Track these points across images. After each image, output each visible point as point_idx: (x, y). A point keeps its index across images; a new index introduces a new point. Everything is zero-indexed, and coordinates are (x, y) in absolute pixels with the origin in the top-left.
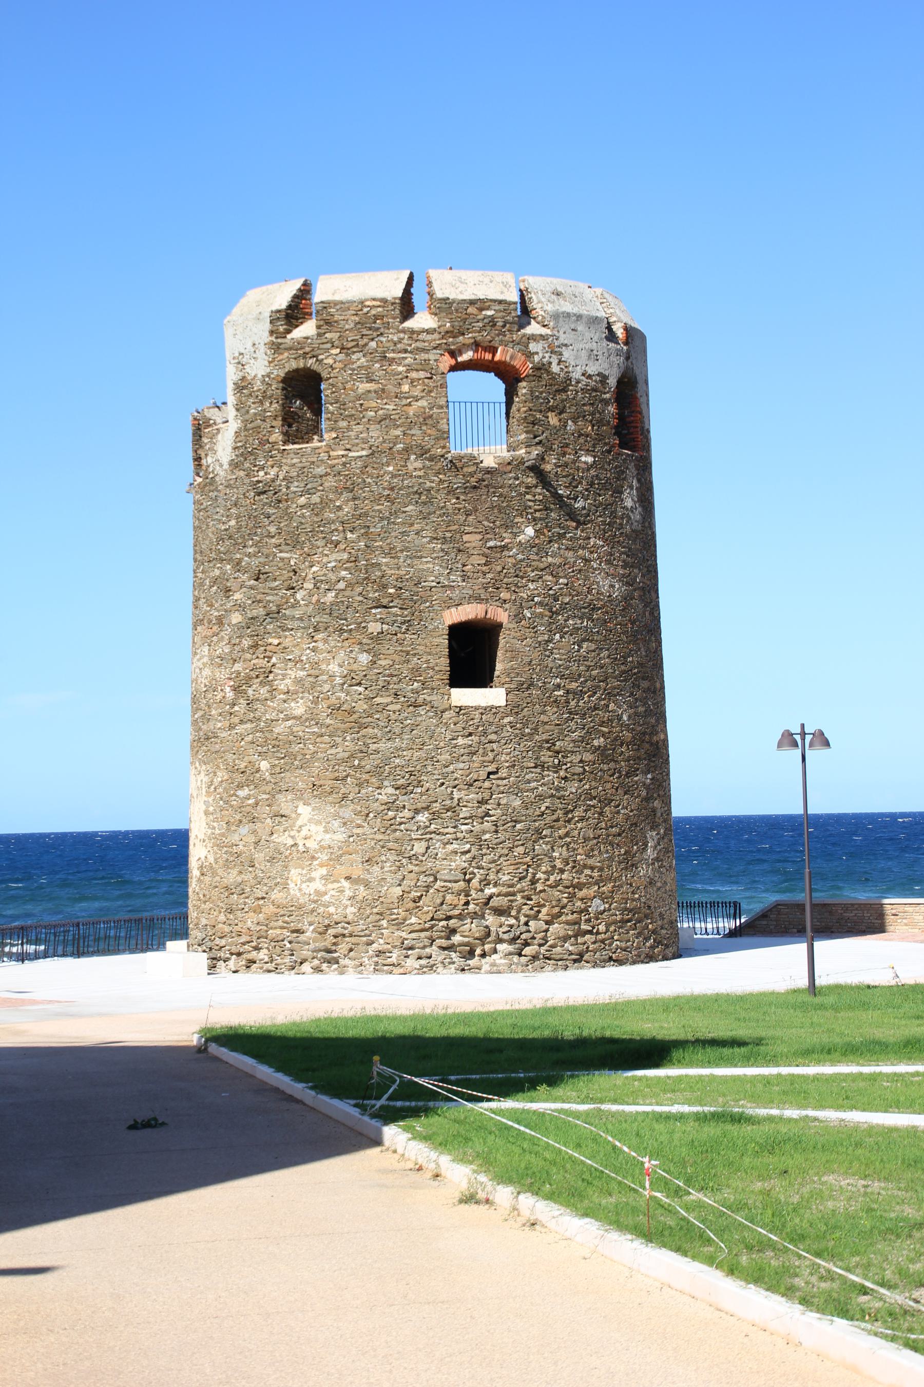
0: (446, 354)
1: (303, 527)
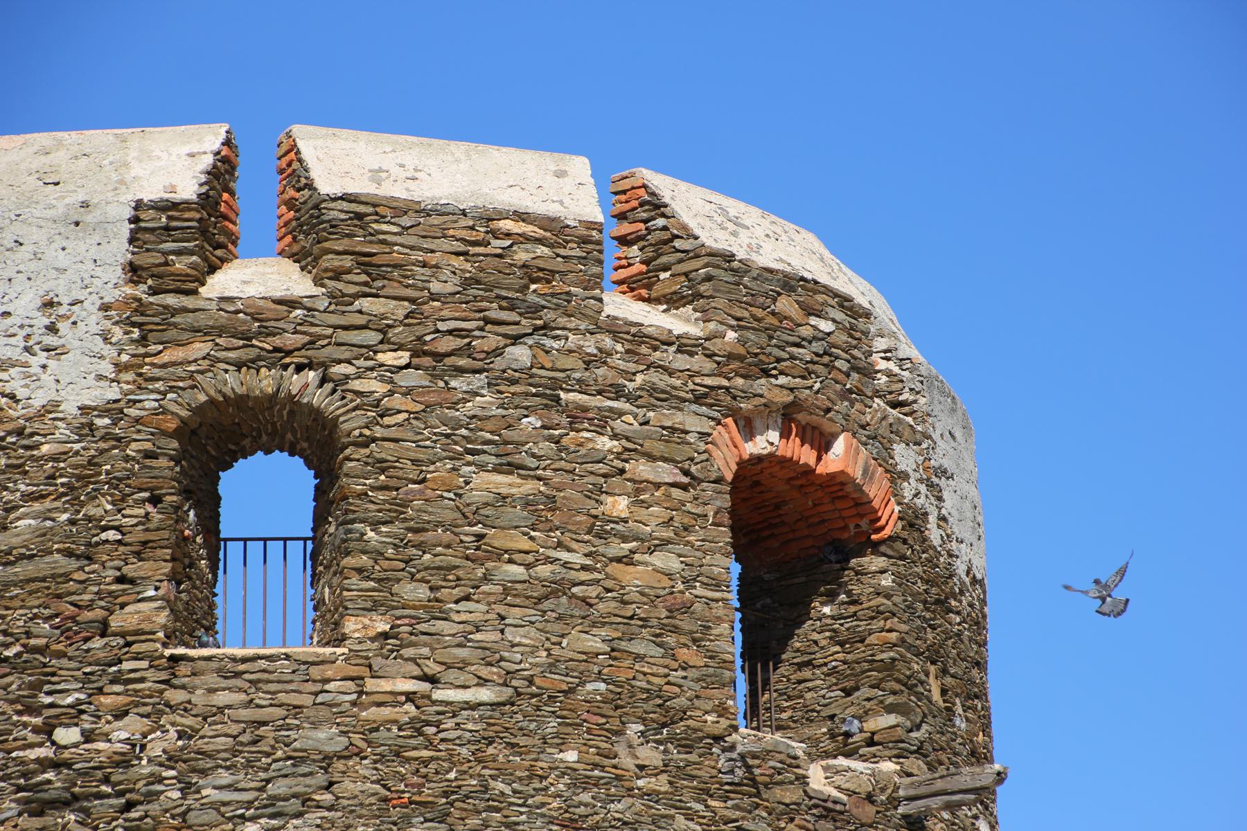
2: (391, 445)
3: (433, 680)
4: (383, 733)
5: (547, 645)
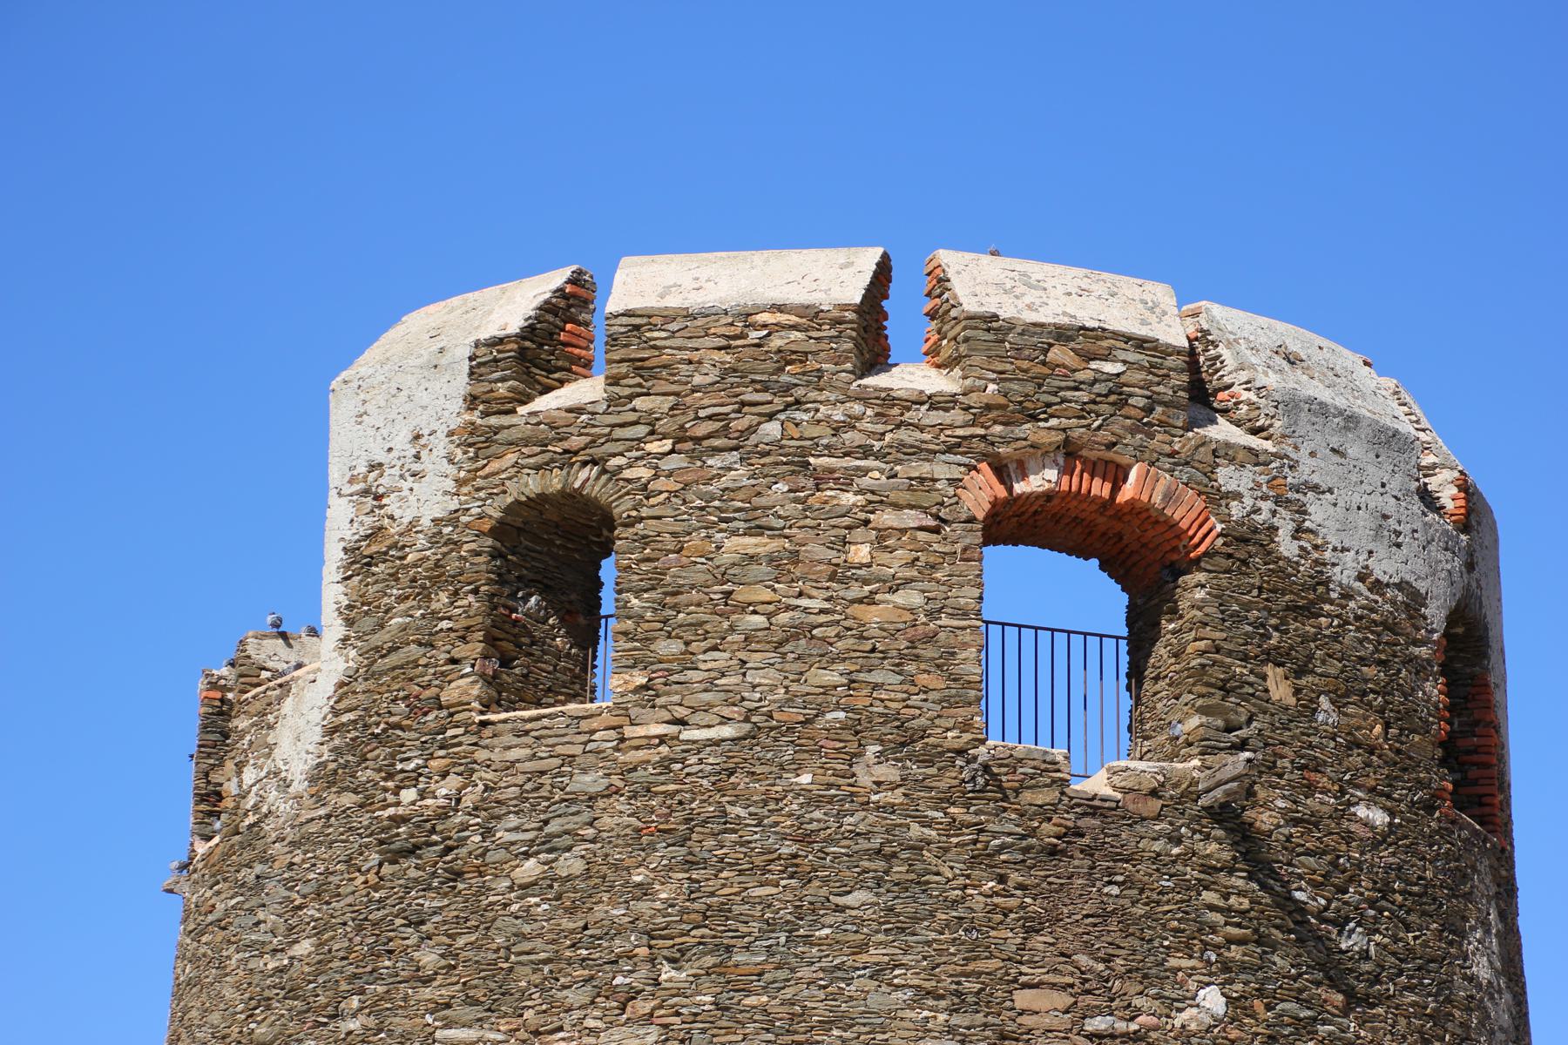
0: (984, 466)
1: (527, 946)
2: (654, 522)
3: (682, 722)
4: (640, 772)
5: (786, 683)
